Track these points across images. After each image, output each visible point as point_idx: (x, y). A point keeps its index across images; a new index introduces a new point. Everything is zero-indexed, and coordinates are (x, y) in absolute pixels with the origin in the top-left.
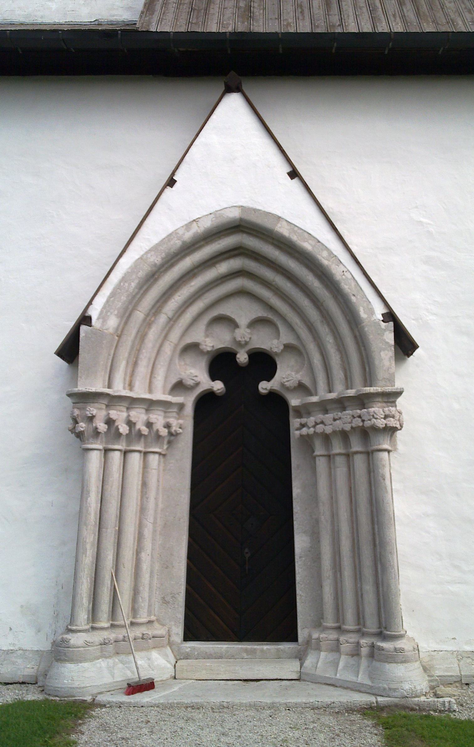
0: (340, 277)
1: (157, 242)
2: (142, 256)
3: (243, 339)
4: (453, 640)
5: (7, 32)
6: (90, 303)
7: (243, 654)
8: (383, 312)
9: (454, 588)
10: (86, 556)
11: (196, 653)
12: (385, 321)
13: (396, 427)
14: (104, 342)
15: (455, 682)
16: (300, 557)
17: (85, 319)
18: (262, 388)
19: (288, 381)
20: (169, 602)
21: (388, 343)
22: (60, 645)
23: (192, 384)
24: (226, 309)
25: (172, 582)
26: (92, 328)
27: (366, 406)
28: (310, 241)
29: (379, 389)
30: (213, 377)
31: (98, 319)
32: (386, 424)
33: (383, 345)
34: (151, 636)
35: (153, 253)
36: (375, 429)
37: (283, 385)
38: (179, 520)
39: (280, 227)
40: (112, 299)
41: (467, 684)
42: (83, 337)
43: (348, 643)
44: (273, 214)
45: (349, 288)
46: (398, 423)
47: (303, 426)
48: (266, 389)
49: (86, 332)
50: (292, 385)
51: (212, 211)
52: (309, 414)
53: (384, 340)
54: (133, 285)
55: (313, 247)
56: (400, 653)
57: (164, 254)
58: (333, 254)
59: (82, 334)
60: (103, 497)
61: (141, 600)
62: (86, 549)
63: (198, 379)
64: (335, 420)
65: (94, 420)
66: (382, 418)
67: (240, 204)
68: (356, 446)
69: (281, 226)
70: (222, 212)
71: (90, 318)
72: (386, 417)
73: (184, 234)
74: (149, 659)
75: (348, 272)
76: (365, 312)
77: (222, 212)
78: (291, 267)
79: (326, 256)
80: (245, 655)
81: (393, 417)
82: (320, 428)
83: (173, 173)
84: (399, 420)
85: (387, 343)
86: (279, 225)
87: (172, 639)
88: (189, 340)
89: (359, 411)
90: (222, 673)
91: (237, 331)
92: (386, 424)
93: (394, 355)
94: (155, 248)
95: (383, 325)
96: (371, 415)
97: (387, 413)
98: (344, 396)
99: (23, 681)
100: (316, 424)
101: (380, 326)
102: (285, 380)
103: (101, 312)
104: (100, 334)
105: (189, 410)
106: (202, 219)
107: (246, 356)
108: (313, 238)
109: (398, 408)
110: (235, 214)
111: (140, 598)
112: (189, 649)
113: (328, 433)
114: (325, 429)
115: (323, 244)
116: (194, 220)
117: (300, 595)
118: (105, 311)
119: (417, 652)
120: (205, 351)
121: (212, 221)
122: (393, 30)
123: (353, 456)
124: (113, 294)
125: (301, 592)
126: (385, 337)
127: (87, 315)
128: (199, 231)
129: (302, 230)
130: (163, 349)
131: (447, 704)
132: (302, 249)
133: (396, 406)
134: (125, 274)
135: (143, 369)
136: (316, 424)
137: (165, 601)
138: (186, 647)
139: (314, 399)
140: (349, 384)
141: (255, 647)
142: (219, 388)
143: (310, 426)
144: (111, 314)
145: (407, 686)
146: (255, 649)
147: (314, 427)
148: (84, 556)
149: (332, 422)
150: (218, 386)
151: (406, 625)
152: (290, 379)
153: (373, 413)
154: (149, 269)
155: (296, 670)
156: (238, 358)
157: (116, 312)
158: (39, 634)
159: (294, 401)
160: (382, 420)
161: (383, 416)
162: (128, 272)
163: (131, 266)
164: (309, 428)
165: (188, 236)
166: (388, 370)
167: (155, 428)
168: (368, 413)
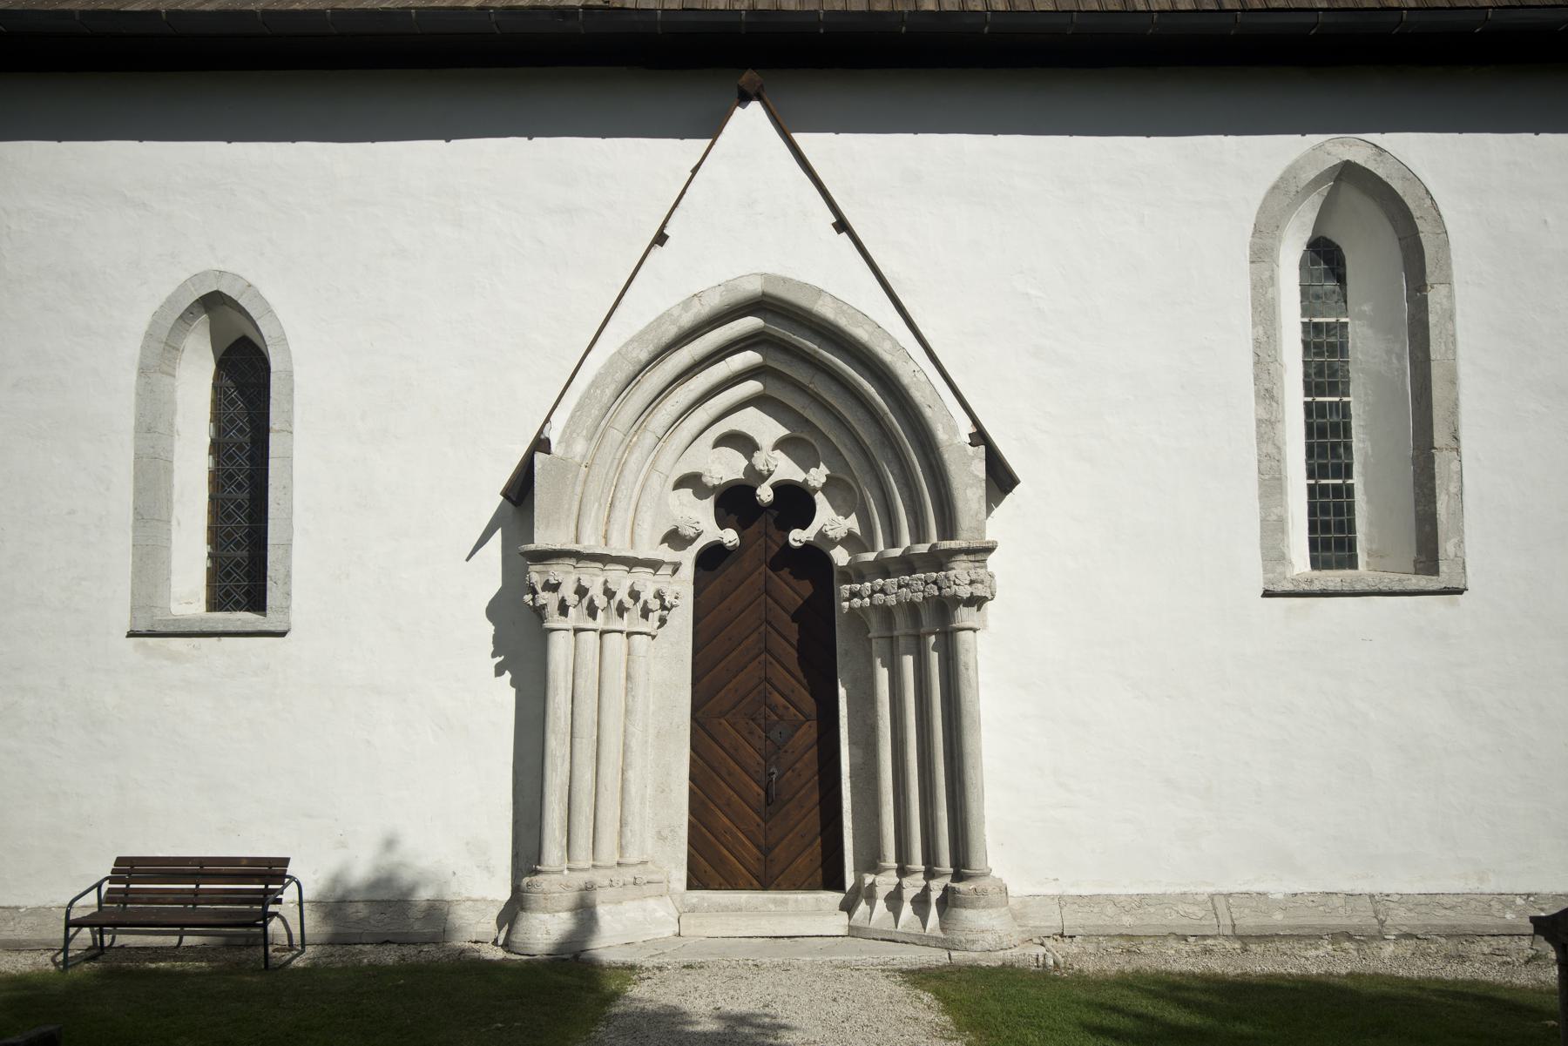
0: (910, 380)
2: (621, 349)
4: (1054, 883)
6: (547, 420)
10: (557, 774)
11: (706, 905)
13: (985, 597)
14: (569, 476)
17: (541, 444)
18: (794, 540)
23: (692, 535)
27: (944, 568)
28: (866, 327)
30: (722, 524)
31: (560, 442)
32: (972, 593)
34: (645, 881)
36: (957, 601)
38: (678, 727)
39: (821, 306)
40: (578, 413)
41: (1070, 937)
45: (922, 396)
46: (989, 590)
47: (854, 595)
51: (722, 280)
55: (871, 334)
60: (576, 696)
61: (629, 834)
62: (557, 765)
63: (700, 527)
64: (900, 587)
65: (1262, 593)
67: (764, 270)
70: (737, 282)
71: (548, 441)
72: (972, 582)
73: (680, 316)
74: (645, 910)
77: (737, 282)
80: (772, 907)
81: (982, 582)
82: (879, 597)
84: (990, 587)
85: (976, 476)
86: (820, 302)
87: (671, 886)
89: (935, 575)
92: (972, 593)
94: (639, 338)
97: (974, 577)
101: (966, 451)
103: (564, 432)
104: (564, 465)
105: (688, 570)
106: (706, 293)
107: (771, 492)
108: (869, 322)
109: (989, 569)
110: (753, 287)
111: (629, 831)
115: (885, 331)
118: (568, 432)
119: (1005, 894)
120: (710, 485)
121: (721, 296)
122: (991, 6)
123: (925, 638)
124: (580, 406)
126: (973, 468)
127: (542, 437)
128: (702, 311)
129: (855, 309)
130: (649, 482)
131: (1041, 959)
132: (854, 338)
133: (986, 567)
134: (596, 377)
135: (622, 516)
137: (660, 836)
138: (693, 897)
140: (919, 534)
143: (864, 595)
144: (578, 435)
145: (989, 937)
146: (786, 899)
147: (870, 597)
148: (554, 774)
150: (730, 537)
151: (992, 862)
155: (843, 923)
157: (584, 432)
159: (840, 557)
160: (967, 587)
161: (968, 582)
162: (600, 374)
163: (605, 364)
164: (862, 598)
167: (643, 597)
168: (947, 578)
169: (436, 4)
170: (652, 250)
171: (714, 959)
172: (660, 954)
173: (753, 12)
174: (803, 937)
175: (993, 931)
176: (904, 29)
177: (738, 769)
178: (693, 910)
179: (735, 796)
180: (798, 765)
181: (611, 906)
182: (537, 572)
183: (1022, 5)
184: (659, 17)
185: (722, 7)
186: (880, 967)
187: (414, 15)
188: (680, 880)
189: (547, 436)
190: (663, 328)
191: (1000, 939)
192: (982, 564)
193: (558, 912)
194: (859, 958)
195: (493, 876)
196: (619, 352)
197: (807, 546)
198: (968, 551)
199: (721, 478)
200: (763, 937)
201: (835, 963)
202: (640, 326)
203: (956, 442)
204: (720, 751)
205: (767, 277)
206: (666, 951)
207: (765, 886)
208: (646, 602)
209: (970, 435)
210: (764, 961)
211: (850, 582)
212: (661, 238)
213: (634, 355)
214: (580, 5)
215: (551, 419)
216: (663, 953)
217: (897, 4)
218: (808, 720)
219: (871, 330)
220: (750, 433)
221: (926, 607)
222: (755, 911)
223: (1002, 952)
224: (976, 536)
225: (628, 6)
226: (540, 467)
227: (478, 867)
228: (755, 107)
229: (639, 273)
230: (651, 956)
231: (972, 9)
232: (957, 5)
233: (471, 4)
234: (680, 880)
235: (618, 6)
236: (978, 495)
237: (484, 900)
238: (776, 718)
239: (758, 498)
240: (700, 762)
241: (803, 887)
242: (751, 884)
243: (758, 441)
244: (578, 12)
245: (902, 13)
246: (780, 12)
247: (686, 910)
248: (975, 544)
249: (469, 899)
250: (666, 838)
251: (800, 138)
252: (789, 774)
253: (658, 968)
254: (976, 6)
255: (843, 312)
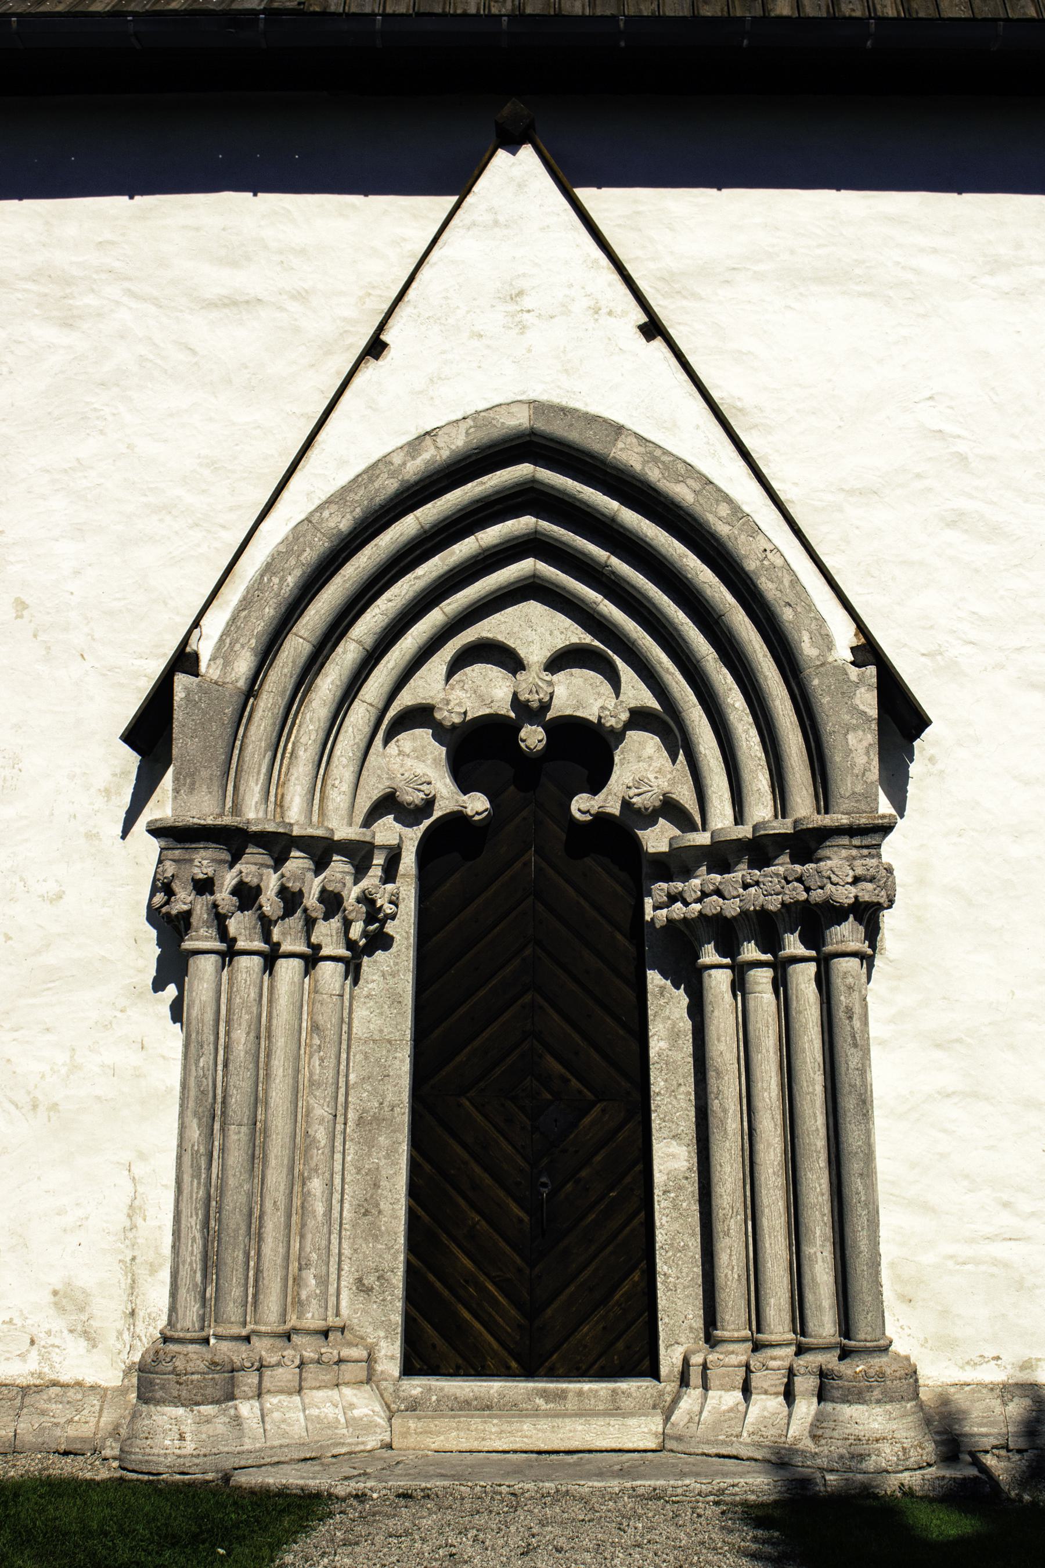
1: (344, 484)
2: (312, 514)
3: (537, 697)
4: (993, 1362)
5: (11, 21)
6: (196, 624)
7: (537, 1401)
8: (854, 645)
9: (1001, 1250)
11: (434, 1398)
12: (857, 662)
13: (879, 904)
15: (995, 1447)
16: (665, 1192)
18: (579, 810)
19: (639, 795)
20: (371, 1289)
21: (865, 713)
22: (152, 1369)
24: (488, 628)
25: (380, 1246)
26: (200, 678)
28: (690, 482)
29: (845, 820)
31: (213, 658)
33: (852, 718)
35: (333, 508)
37: (626, 804)
38: (392, 1110)
39: (621, 450)
40: (244, 614)
42: (182, 699)
43: (767, 1369)
44: (605, 421)
48: (588, 811)
49: (188, 691)
50: (649, 804)
51: (470, 410)
52: (687, 874)
53: (855, 708)
54: (291, 580)
56: (875, 1383)
57: (358, 510)
58: (742, 511)
59: (179, 694)
64: (746, 886)
66: (848, 883)
67: (532, 396)
68: (793, 945)
69: (623, 446)
71: (195, 657)
72: (856, 880)
73: (404, 464)
75: (775, 550)
76: (813, 643)
78: (646, 536)
79: (725, 515)
80: (540, 1401)
83: (381, 327)
87: (379, 1368)
88: (406, 699)
90: (493, 1437)
91: (521, 676)
92: (856, 897)
93: (876, 741)
94: (339, 498)
95: (854, 672)
96: (823, 877)
97: (860, 871)
98: (766, 832)
99: (67, 1450)
100: (704, 895)
102: (632, 792)
103: (221, 640)
110: (519, 420)
112: (419, 1390)
113: (729, 915)
114: (724, 907)
115: (719, 490)
116: (428, 433)
117: (665, 1275)
118: (228, 641)
120: (447, 723)
121: (467, 434)
124: (246, 603)
125: (665, 1268)
126: (857, 701)
133: (879, 856)
136: (704, 895)
137: (362, 1287)
139: (703, 839)
141: (564, 1385)
142: (480, 809)
143: (689, 900)
144: (243, 646)
146: (564, 1391)
149: (741, 890)
150: (477, 804)
152: (645, 789)
153: (829, 872)
154: (326, 544)
156: (523, 741)
158: (95, 1350)
161: (850, 880)
165: (414, 468)
166: (864, 774)
169: (46, 7)
170: (362, 365)
171: (446, 1483)
172: (359, 1475)
173: (518, 17)
174: (590, 1451)
175: (894, 1441)
176: (745, 42)
177: (488, 1180)
178: (414, 1406)
179: (483, 1223)
180: (584, 1173)
181: (282, 1397)
182: (174, 861)
183: (852, 7)
184: (378, 26)
185: (473, 10)
186: (711, 1498)
187: (14, 25)
188: (392, 1358)
189: (196, 648)
190: (377, 485)
191: (904, 1454)
192: (873, 851)
193: (197, 1404)
194: (680, 1483)
195: (94, 1346)
196: (308, 519)
197: (601, 818)
198: (851, 831)
199: (465, 713)
200: (526, 1452)
201: (641, 1491)
202: (344, 478)
203: (830, 659)
204: (459, 1149)
205: (538, 407)
206: (368, 1470)
207: (529, 1373)
208: (356, 883)
209: (852, 649)
210: (527, 1486)
211: (668, 879)
212: (376, 348)
213: (332, 525)
214: (262, 7)
215: (202, 623)
216: (365, 1474)
217: (734, 7)
218: (600, 1101)
219: (697, 486)
220: (511, 643)
221: (787, 919)
222: (512, 1410)
223: (907, 1474)
224: (863, 806)
225: (333, 9)
226: (183, 695)
227: (71, 1331)
228: (527, 153)
229: (333, 415)
230: (346, 1478)
231: (847, 15)
232: (824, 9)
233: (97, 7)
234: (392, 1358)
235: (317, 9)
236: (865, 744)
237: (79, 1384)
238: (549, 1097)
239: (522, 745)
240: (427, 1167)
241: (592, 1372)
242: (508, 1368)
243: (522, 655)
244: (375, 20)
245: (742, 19)
246: (560, 17)
247: (403, 1407)
248: (863, 821)
249: (55, 1384)
250: (371, 1289)
251: (583, 194)
252: (569, 1186)
253: (356, 1496)
254: (853, 10)
255: (655, 460)
